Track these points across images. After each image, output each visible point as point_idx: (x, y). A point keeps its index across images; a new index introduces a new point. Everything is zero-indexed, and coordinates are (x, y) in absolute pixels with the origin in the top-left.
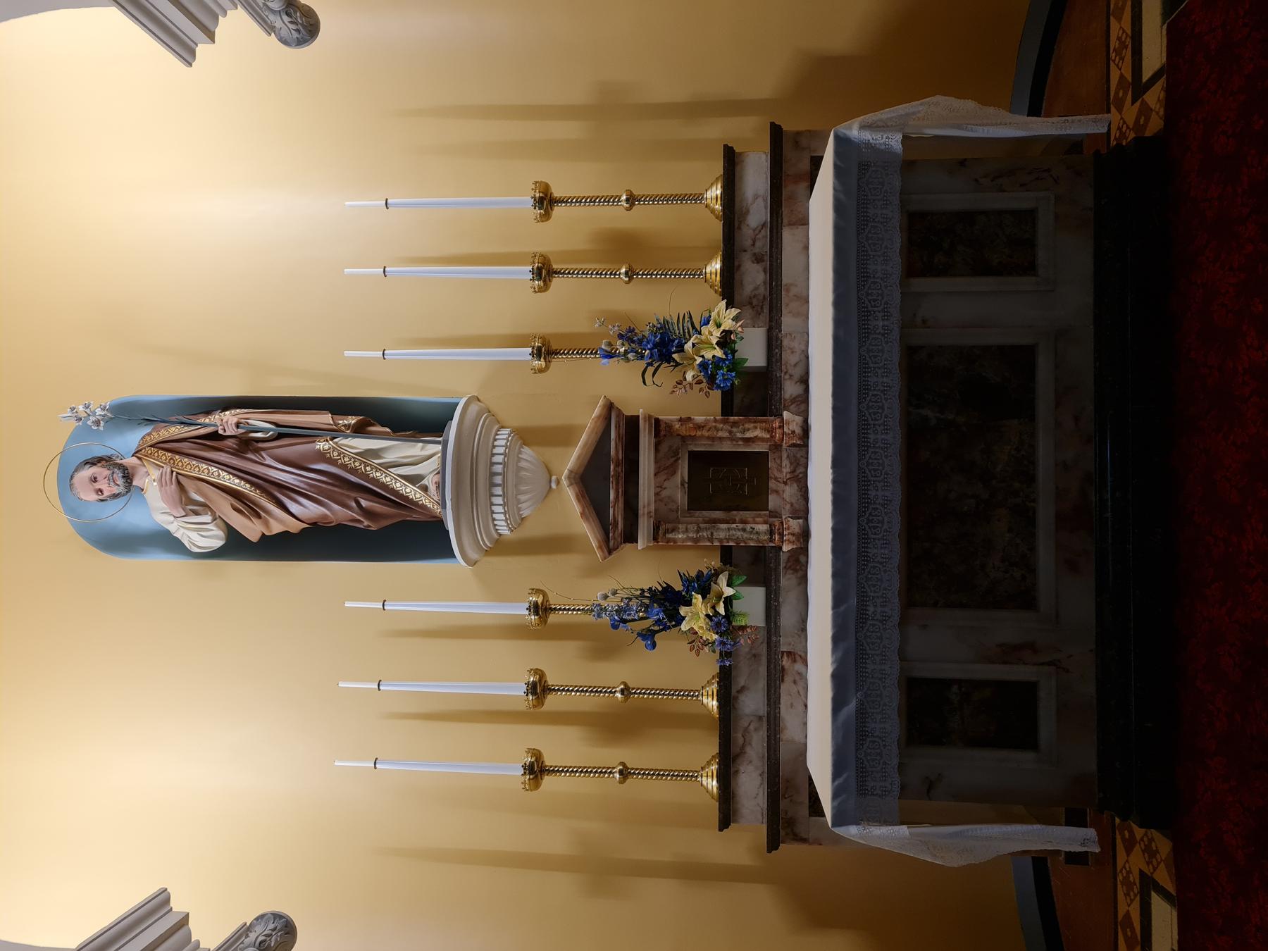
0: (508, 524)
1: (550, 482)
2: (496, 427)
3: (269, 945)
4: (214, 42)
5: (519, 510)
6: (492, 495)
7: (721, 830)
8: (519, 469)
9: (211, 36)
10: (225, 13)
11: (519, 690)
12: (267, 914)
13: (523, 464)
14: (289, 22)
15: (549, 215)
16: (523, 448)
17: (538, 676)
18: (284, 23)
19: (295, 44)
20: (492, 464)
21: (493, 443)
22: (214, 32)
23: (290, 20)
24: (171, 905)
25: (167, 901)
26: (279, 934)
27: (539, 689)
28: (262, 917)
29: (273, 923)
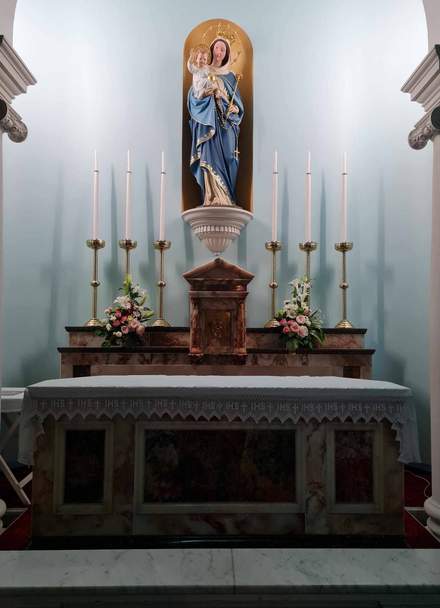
0: (201, 233)
1: (217, 252)
2: (240, 229)
3: (14, 131)
4: (412, 101)
5: (205, 238)
6: (211, 226)
7: (66, 328)
8: (222, 239)
9: (415, 99)
10: (424, 106)
11: (161, 239)
12: (27, 130)
13: (224, 240)
14: (419, 137)
15: (302, 249)
16: (232, 240)
17: (133, 245)
18: (419, 134)
19: (410, 139)
20: (224, 226)
21: (236, 227)
22: (416, 101)
23: (420, 137)
24: (30, 86)
25: (32, 84)
26: (19, 135)
27: (128, 245)
28: (26, 127)
29: (23, 132)
